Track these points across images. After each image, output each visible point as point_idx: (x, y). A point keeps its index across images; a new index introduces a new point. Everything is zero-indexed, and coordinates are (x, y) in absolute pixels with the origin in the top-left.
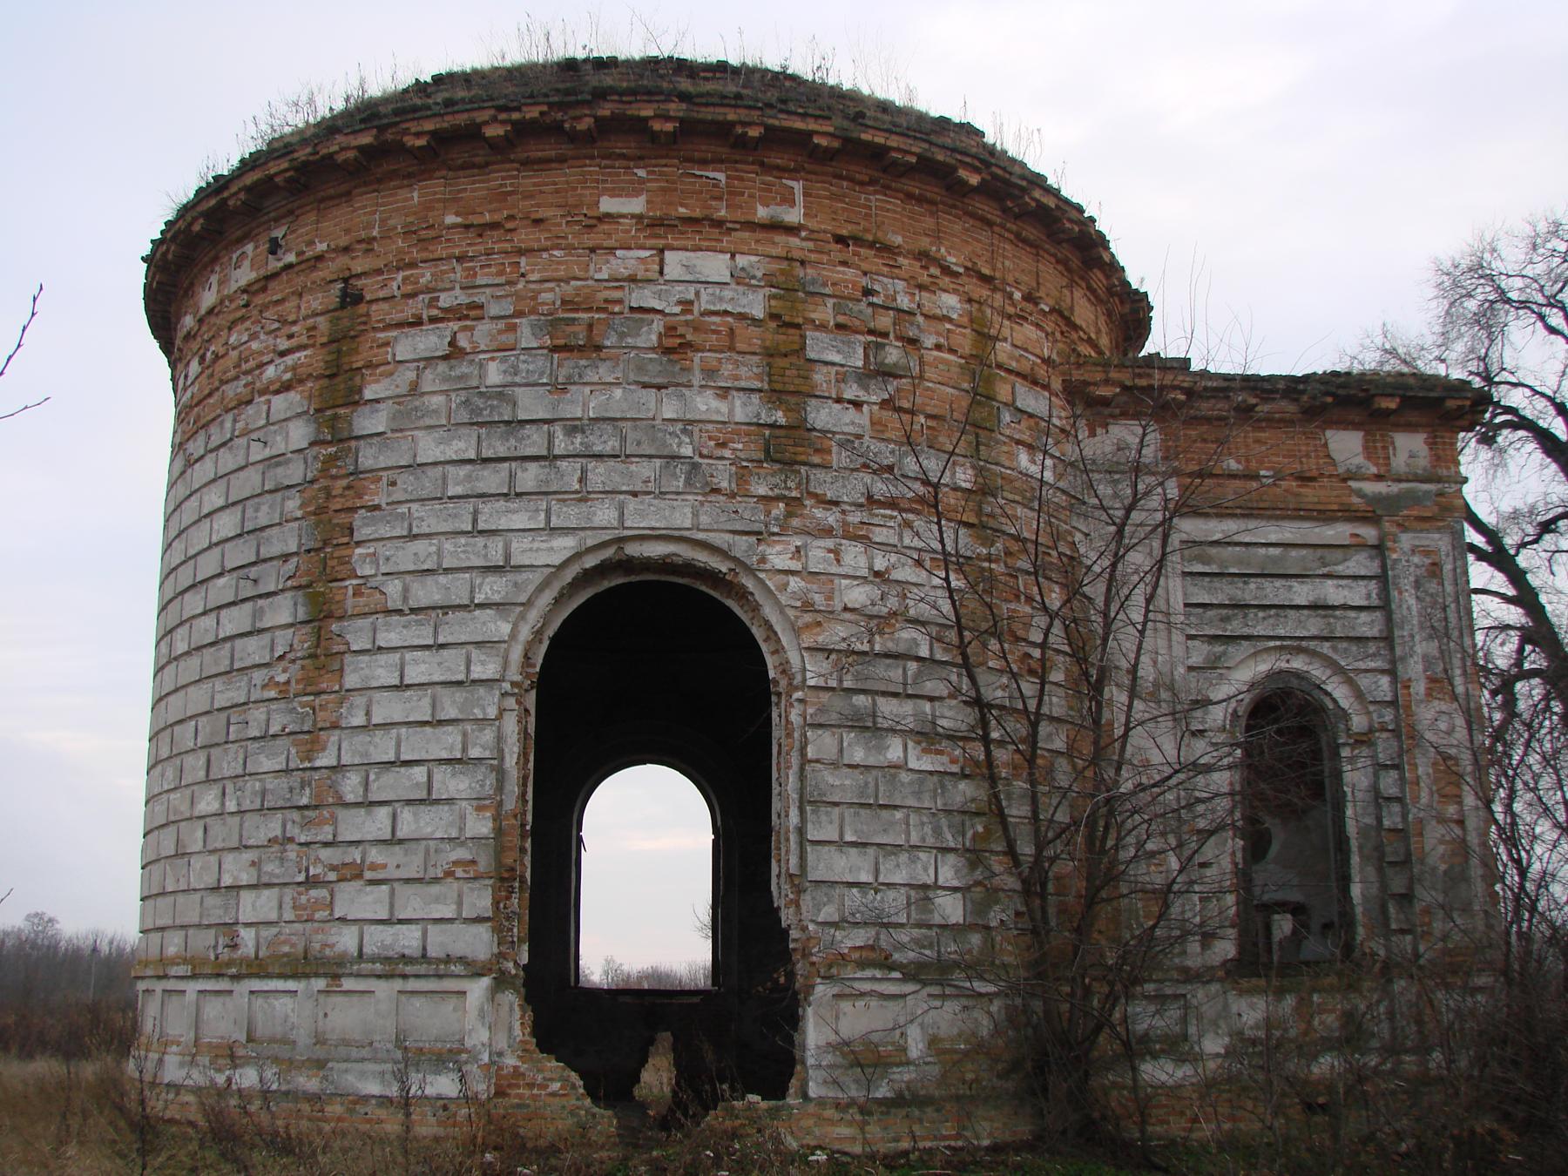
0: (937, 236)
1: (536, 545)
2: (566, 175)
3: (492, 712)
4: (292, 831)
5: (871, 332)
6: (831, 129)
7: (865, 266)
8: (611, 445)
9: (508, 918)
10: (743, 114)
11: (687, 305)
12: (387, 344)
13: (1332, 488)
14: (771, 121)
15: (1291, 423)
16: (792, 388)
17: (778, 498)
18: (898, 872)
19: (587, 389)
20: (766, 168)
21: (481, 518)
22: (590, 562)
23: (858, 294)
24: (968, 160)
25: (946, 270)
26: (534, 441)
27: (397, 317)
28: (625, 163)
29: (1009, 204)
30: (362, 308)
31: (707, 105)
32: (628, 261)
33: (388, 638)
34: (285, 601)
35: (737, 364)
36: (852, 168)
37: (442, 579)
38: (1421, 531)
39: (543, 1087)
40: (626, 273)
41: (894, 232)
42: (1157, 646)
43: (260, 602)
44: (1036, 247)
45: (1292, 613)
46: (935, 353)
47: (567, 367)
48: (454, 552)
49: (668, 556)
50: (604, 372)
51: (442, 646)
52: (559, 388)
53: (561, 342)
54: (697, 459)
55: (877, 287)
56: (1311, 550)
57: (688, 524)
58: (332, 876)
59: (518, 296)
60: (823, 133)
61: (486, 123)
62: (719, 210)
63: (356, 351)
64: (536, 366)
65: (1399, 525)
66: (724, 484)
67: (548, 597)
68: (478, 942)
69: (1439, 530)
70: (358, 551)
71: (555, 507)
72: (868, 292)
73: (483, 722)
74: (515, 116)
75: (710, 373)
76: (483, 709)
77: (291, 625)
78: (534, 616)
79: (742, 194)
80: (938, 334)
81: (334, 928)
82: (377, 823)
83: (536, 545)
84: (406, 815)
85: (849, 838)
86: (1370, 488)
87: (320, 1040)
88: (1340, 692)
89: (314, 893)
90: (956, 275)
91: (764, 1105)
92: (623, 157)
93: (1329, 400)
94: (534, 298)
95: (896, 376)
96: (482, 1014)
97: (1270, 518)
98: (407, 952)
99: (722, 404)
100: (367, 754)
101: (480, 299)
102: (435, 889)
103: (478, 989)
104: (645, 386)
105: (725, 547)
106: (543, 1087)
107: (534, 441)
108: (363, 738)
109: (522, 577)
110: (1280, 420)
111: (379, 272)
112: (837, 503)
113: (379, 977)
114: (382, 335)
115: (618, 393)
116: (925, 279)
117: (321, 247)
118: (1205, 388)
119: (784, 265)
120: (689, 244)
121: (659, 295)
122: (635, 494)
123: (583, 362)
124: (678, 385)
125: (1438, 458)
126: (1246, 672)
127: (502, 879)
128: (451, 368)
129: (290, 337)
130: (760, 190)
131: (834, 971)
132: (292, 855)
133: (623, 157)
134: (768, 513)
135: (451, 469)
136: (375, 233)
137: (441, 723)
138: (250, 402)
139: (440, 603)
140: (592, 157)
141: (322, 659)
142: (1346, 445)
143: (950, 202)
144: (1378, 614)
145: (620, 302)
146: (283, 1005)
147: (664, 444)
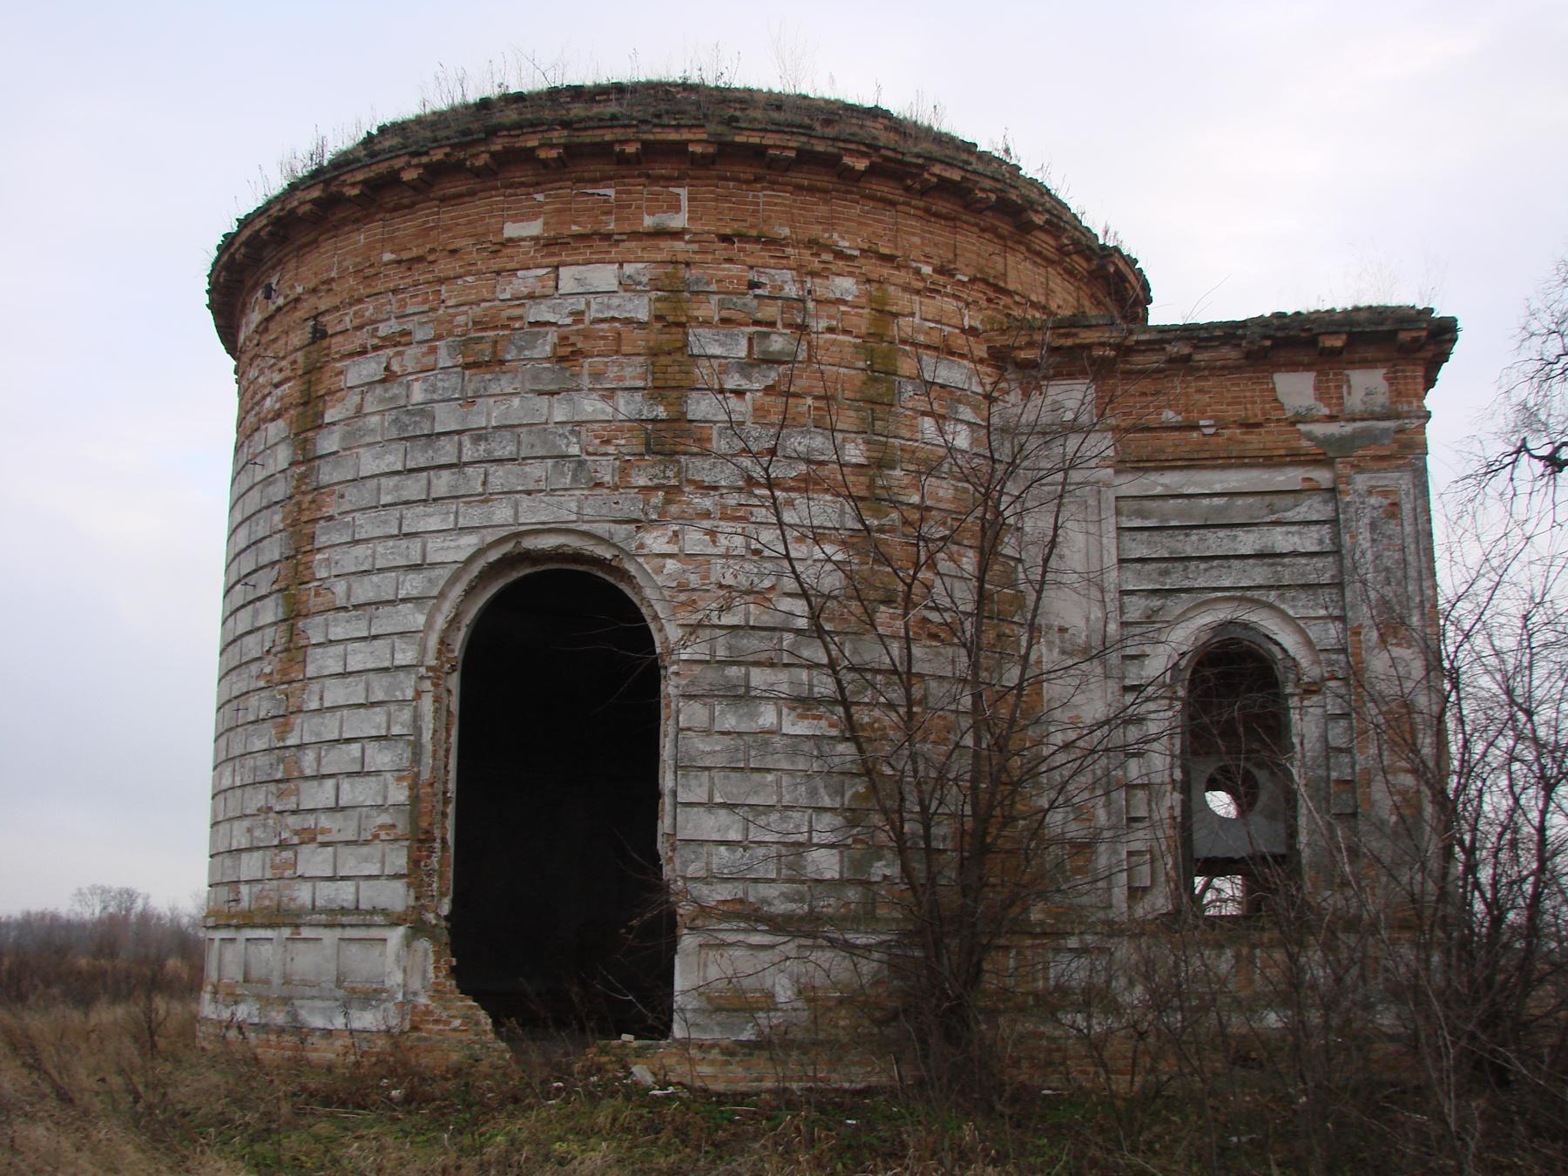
0: (830, 223)
1: (447, 544)
2: (474, 208)
3: (410, 694)
4: (272, 802)
5: (757, 323)
6: (704, 137)
7: (750, 261)
8: (509, 450)
9: (429, 875)
10: (619, 133)
11: (578, 315)
12: (341, 373)
13: (1280, 433)
14: (646, 137)
15: (1238, 369)
16: (674, 384)
17: (657, 488)
18: (768, 831)
19: (491, 401)
20: (655, 180)
21: (405, 522)
22: (493, 556)
23: (743, 288)
24: (853, 146)
25: (839, 255)
26: (446, 451)
27: (349, 348)
28: (524, 190)
29: (909, 182)
30: (325, 343)
31: (585, 129)
32: (527, 280)
33: (337, 632)
34: (270, 603)
35: (621, 366)
36: (736, 169)
37: (375, 578)
38: (1378, 471)
39: (447, 1023)
40: (526, 291)
41: (781, 225)
42: (1082, 563)
43: (258, 604)
44: (953, 219)
45: (1236, 563)
46: (828, 336)
47: (474, 381)
48: (388, 554)
49: (559, 547)
50: (505, 384)
51: (375, 637)
52: (469, 401)
53: (471, 360)
54: (584, 457)
55: (763, 280)
56: (1258, 498)
57: (573, 517)
58: (296, 840)
59: (439, 321)
60: (697, 141)
61: (403, 169)
62: (607, 224)
63: (319, 381)
64: (449, 383)
65: (1353, 466)
66: (607, 478)
67: (458, 591)
68: (396, 896)
69: (1398, 468)
70: (318, 557)
71: (462, 509)
72: (753, 285)
73: (402, 702)
74: (425, 160)
75: (597, 376)
76: (403, 691)
77: (275, 623)
78: (448, 608)
79: (630, 206)
80: (830, 317)
81: (297, 885)
82: (323, 795)
83: (447, 544)
84: (346, 785)
85: (718, 800)
86: (1320, 429)
87: (287, 981)
88: (1288, 639)
89: (284, 854)
90: (851, 258)
91: (636, 1044)
92: (522, 184)
93: (1268, 343)
94: (451, 322)
95: (780, 363)
96: (398, 960)
97: (1215, 467)
98: (345, 904)
99: (608, 404)
100: (319, 734)
101: (409, 327)
102: (365, 850)
103: (396, 935)
104: (540, 393)
105: (606, 536)
106: (447, 1023)
107: (446, 451)
108: (316, 720)
109: (438, 572)
110: (1223, 368)
111: (337, 308)
112: (715, 488)
113: (325, 926)
114: (338, 365)
115: (516, 401)
116: (816, 265)
117: (299, 290)
118: (1137, 342)
119: (670, 269)
120: (580, 258)
121: (553, 310)
122: (529, 493)
123: (488, 377)
124: (568, 390)
125: (1399, 394)
126: (1186, 633)
127: (420, 841)
128: (386, 391)
129: (281, 370)
130: (648, 200)
131: (699, 922)
132: (271, 822)
133: (522, 184)
134: (646, 502)
135: (383, 480)
136: (333, 275)
137: (373, 704)
138: (258, 429)
139: (374, 600)
140: (497, 189)
141: (294, 650)
142: (1295, 389)
143: (843, 188)
144: (1331, 559)
145: (520, 318)
146: (267, 949)
147: (555, 446)
